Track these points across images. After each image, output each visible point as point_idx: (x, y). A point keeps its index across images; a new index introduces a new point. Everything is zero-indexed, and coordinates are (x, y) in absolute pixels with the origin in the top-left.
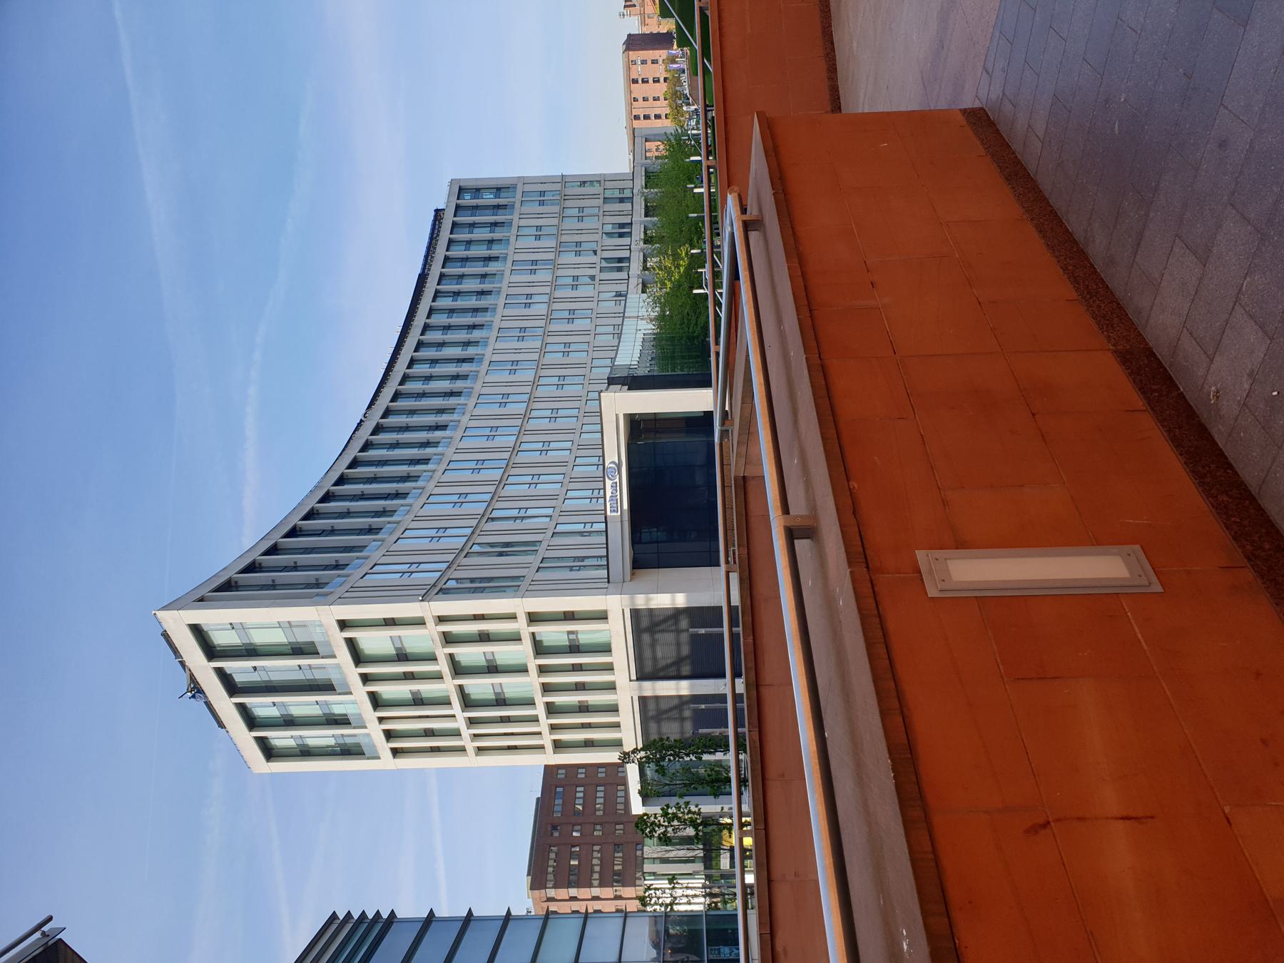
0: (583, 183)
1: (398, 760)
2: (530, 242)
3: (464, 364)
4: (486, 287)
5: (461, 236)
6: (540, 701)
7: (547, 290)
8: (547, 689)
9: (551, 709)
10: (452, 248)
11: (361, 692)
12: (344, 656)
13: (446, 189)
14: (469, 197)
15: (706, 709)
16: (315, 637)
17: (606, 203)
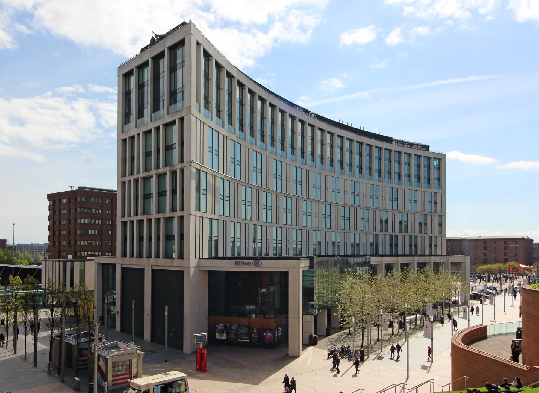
0: (440, 225)
1: (121, 142)
2: (408, 197)
3: (339, 164)
4: (383, 173)
5: (413, 161)
6: (145, 218)
7: (381, 206)
8: (150, 221)
9: (141, 222)
10: (406, 155)
11: (151, 126)
12: (168, 120)
13: (440, 151)
14: (425, 176)
15: (132, 308)
16: (179, 105)
17: (439, 217)
